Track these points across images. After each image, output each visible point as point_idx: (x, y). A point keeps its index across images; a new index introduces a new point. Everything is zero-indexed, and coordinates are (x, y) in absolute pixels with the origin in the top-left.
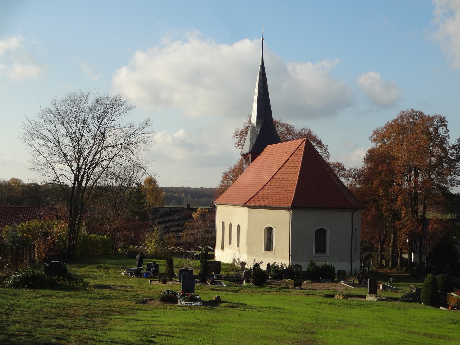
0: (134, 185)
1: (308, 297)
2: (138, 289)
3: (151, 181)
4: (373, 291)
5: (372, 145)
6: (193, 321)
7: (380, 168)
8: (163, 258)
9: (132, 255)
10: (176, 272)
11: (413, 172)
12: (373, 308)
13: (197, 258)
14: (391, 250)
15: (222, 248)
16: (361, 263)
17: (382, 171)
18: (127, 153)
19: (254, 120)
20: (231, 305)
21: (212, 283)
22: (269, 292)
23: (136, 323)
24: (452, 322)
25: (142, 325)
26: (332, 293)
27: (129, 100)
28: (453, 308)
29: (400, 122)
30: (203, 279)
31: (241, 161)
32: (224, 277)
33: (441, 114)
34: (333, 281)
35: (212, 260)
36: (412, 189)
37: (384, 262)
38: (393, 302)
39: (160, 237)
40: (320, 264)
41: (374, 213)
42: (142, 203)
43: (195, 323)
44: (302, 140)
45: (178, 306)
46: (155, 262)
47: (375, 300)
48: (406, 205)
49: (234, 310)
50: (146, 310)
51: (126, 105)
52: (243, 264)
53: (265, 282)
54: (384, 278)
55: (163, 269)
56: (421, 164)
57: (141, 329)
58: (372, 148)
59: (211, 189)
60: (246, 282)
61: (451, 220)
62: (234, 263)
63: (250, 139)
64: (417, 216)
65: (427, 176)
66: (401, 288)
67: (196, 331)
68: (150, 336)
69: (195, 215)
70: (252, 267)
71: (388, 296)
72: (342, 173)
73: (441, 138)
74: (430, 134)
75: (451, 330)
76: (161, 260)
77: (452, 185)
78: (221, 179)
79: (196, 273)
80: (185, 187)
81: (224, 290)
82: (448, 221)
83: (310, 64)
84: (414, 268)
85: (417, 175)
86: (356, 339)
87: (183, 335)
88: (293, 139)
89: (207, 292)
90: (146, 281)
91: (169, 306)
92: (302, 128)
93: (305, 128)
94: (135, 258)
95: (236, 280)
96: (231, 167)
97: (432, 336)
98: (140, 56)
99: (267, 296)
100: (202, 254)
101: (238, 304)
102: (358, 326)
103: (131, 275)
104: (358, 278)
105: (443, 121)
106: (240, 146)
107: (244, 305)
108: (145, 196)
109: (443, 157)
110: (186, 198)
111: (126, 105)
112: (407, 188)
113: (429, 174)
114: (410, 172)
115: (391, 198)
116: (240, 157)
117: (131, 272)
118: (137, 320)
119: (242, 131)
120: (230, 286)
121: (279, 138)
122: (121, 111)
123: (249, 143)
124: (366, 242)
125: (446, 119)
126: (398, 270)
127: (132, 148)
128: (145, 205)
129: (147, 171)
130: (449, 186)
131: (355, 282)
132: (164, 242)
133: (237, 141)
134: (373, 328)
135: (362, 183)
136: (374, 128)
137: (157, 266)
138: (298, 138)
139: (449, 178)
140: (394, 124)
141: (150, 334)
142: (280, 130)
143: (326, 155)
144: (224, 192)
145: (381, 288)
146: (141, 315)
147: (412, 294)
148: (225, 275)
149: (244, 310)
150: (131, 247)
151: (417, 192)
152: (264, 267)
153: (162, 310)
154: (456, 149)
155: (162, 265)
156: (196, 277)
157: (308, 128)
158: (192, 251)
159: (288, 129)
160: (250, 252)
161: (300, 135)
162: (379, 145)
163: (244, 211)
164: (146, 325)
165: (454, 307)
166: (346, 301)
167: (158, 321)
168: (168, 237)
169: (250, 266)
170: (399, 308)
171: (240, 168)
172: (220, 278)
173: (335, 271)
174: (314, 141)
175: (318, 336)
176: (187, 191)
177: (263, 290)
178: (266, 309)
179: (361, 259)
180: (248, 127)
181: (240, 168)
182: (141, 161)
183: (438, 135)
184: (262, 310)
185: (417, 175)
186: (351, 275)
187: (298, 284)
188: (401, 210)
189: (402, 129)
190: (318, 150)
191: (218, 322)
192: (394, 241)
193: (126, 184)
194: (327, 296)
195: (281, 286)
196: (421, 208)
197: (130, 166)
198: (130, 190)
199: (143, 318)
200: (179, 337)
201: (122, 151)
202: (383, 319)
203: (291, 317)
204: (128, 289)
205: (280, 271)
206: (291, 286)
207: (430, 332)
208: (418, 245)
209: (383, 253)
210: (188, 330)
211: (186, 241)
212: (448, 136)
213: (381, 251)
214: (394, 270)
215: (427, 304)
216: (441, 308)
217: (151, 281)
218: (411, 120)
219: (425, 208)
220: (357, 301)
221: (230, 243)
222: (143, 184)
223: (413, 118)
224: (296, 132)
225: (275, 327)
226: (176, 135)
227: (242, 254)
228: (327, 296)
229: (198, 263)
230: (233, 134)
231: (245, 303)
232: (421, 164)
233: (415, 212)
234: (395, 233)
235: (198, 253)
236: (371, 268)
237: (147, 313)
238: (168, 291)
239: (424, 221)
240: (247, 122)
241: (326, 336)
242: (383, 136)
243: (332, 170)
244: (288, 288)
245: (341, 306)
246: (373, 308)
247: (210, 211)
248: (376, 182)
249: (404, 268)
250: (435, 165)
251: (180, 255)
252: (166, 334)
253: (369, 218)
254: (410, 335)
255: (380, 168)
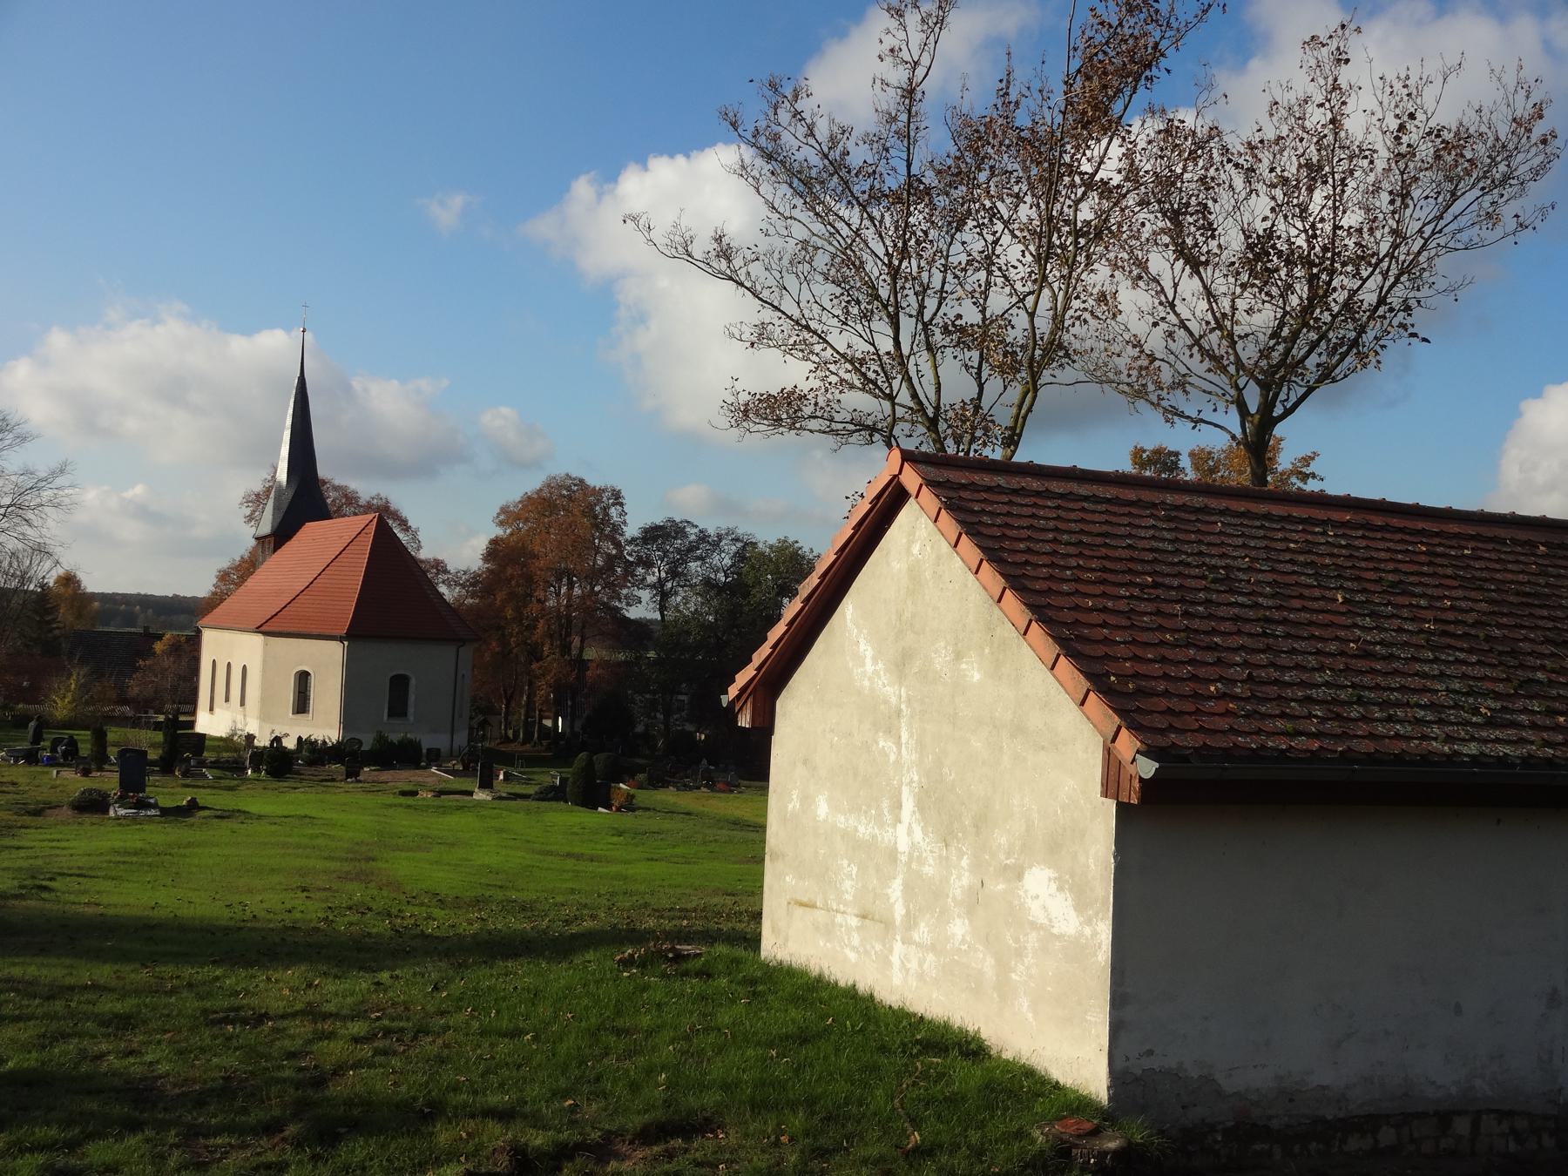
0: (32, 587)
1: (370, 796)
2: (27, 788)
3: (69, 580)
4: (486, 784)
5: (499, 532)
6: (139, 845)
7: (509, 571)
8: (86, 728)
9: (21, 722)
10: (113, 754)
11: (565, 580)
12: (485, 813)
13: (157, 726)
14: (523, 711)
15: (211, 709)
16: (470, 734)
17: (512, 577)
18: (16, 525)
19: (282, 476)
20: (219, 813)
21: (185, 774)
22: (295, 788)
23: (15, 854)
24: (615, 832)
25: (28, 858)
26: (414, 789)
27: (25, 422)
28: (618, 810)
29: (545, 494)
30: (166, 766)
31: (255, 549)
32: (211, 762)
33: (615, 485)
34: (418, 767)
35: (190, 731)
36: (562, 609)
37: (510, 733)
38: (520, 803)
39: (84, 688)
40: (395, 737)
41: (497, 649)
42: (49, 623)
43: (141, 850)
44: (370, 516)
45: (110, 818)
46: (71, 737)
47: (489, 798)
48: (551, 636)
49: (224, 823)
50: (41, 828)
51: (18, 430)
52: (250, 738)
53: (290, 771)
54: (508, 760)
55: (85, 749)
56: (578, 567)
57: (25, 864)
58: (497, 537)
59: (194, 598)
60: (253, 771)
61: (626, 663)
62: (233, 735)
63: (274, 509)
64: (570, 654)
65: (588, 587)
66: (536, 777)
67: (142, 864)
68: (42, 877)
69: (158, 647)
70: (268, 744)
71: (512, 791)
72: (442, 577)
73: (613, 524)
74: (596, 517)
75: (610, 846)
76: (83, 732)
77: (628, 604)
78: (215, 581)
79: (153, 755)
80: (143, 593)
81: (209, 787)
82: (619, 664)
83: (395, 382)
84: (562, 743)
85: (571, 586)
86: (446, 867)
87: (113, 873)
88: (355, 514)
89: (172, 791)
90: (47, 773)
91: (87, 818)
92: (373, 494)
93: (378, 495)
94: (27, 727)
95: (236, 767)
96: (234, 560)
97: (578, 857)
98: (59, 340)
99: (298, 796)
100: (167, 719)
101: (233, 811)
102: (453, 845)
103: (16, 761)
104: (462, 760)
105: (617, 496)
106: (253, 523)
107: (244, 812)
108: (55, 608)
109: (615, 556)
110: (142, 616)
111: (19, 431)
112: (553, 607)
113: (591, 584)
114: (559, 580)
115: (526, 623)
116: (253, 542)
117: (15, 754)
118: (18, 848)
119: (258, 495)
120: (220, 778)
121: (328, 511)
122: (7, 442)
123: (271, 517)
124: (481, 698)
125: (623, 494)
126: (534, 746)
127: (30, 515)
128: (55, 626)
129: (60, 560)
130: (624, 605)
131: (456, 767)
132: (92, 697)
133: (248, 512)
134: (480, 846)
135: (478, 596)
136: (501, 502)
137: (72, 743)
138: (366, 513)
139: (625, 591)
140: (535, 496)
141: (42, 873)
142: (331, 496)
143: (415, 546)
144: (219, 604)
145: (501, 777)
146: (29, 838)
147: (553, 787)
148: (213, 759)
149: (242, 823)
150: (20, 706)
151: (571, 615)
152: (290, 743)
153: (76, 827)
154: (637, 545)
155: (83, 741)
156: (153, 763)
157: (383, 495)
158: (151, 713)
159: (346, 496)
160: (264, 717)
161: (368, 508)
162: (508, 531)
163: (258, 640)
164: (36, 857)
165: (621, 807)
166: (437, 802)
167: (63, 849)
168: (100, 688)
169: (263, 741)
170: (528, 812)
171: (252, 561)
172: (202, 764)
173: (421, 749)
174: (395, 520)
175: (380, 865)
176: (146, 601)
177: (286, 784)
178: (286, 820)
179: (471, 729)
180: (271, 487)
181: (252, 561)
182: (48, 541)
183: (609, 520)
184: (278, 821)
185: (571, 586)
186: (451, 755)
187: (352, 773)
188: (543, 645)
189: (549, 506)
190: (401, 536)
191: (189, 845)
192: (528, 698)
193: (14, 584)
194: (404, 793)
195: (321, 777)
196: (576, 641)
197: (24, 550)
198: (22, 595)
199: (33, 844)
200: (105, 878)
201: (6, 519)
202: (500, 831)
203: (332, 833)
204: (6, 789)
205: (320, 751)
206: (340, 778)
207: (577, 850)
208: (569, 703)
209: (510, 718)
210: (124, 862)
211: (138, 695)
212: (625, 523)
213: (507, 714)
214: (528, 747)
215: (577, 805)
216: (600, 809)
217: (58, 773)
218: (565, 492)
219: (582, 641)
220: (457, 801)
221: (227, 700)
222: (51, 585)
223: (568, 489)
224: (362, 502)
225: (300, 851)
226: (129, 494)
227: (248, 719)
228: (404, 793)
229: (159, 737)
230: (240, 500)
231: (247, 810)
232: (578, 567)
233: (566, 648)
234: (530, 684)
235: (161, 718)
236: (487, 745)
237: (41, 833)
238: (90, 791)
239: (581, 664)
240: (269, 478)
241: (393, 863)
242: (517, 517)
243: (424, 573)
244: (333, 780)
245: (427, 811)
246: (485, 813)
247: (189, 639)
248: (501, 596)
249: (545, 743)
250: (601, 571)
251: (123, 721)
252: (78, 872)
253: (487, 656)
254: (541, 857)
255: (509, 571)
